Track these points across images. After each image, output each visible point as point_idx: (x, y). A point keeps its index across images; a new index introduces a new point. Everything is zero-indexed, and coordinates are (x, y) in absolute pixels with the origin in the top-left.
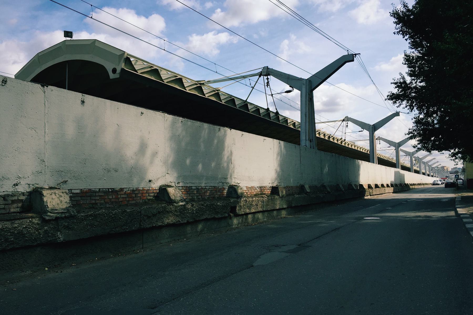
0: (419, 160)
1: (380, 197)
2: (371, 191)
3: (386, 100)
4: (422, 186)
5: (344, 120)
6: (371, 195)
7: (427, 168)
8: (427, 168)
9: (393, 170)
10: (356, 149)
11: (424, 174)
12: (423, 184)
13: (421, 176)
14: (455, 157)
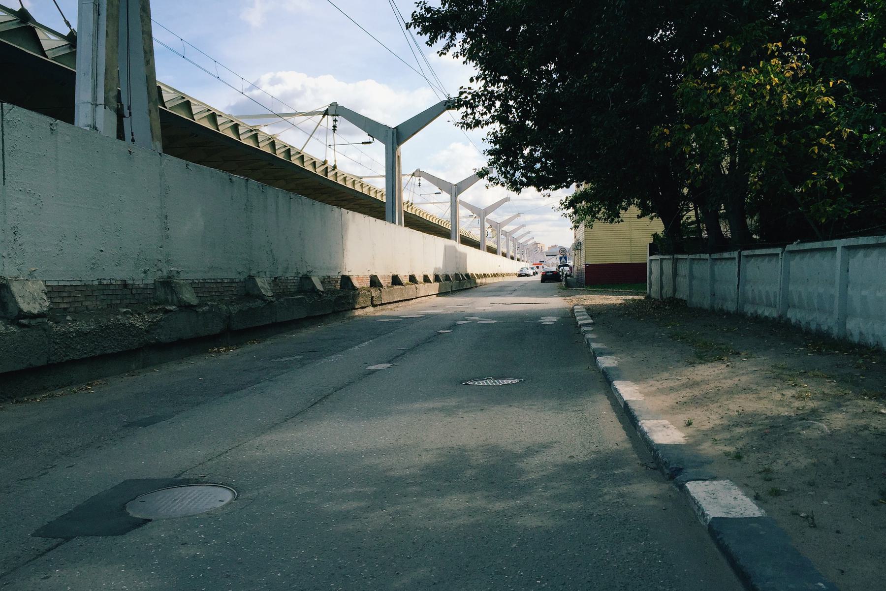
0: (496, 227)
1: (401, 310)
2: (375, 293)
3: (408, 26)
4: (500, 279)
5: (326, 113)
6: (374, 306)
7: (511, 244)
8: (511, 244)
9: (441, 242)
10: (366, 192)
11: (504, 255)
12: (503, 275)
13: (498, 258)
14: (574, 207)
